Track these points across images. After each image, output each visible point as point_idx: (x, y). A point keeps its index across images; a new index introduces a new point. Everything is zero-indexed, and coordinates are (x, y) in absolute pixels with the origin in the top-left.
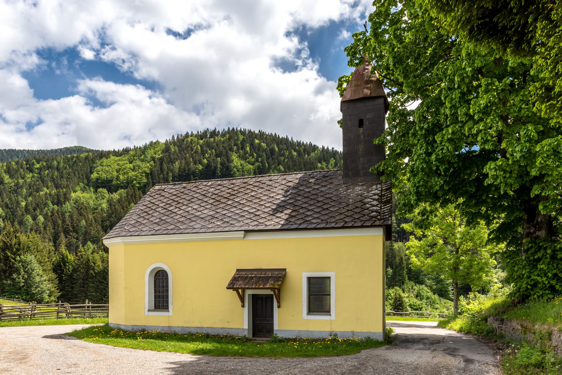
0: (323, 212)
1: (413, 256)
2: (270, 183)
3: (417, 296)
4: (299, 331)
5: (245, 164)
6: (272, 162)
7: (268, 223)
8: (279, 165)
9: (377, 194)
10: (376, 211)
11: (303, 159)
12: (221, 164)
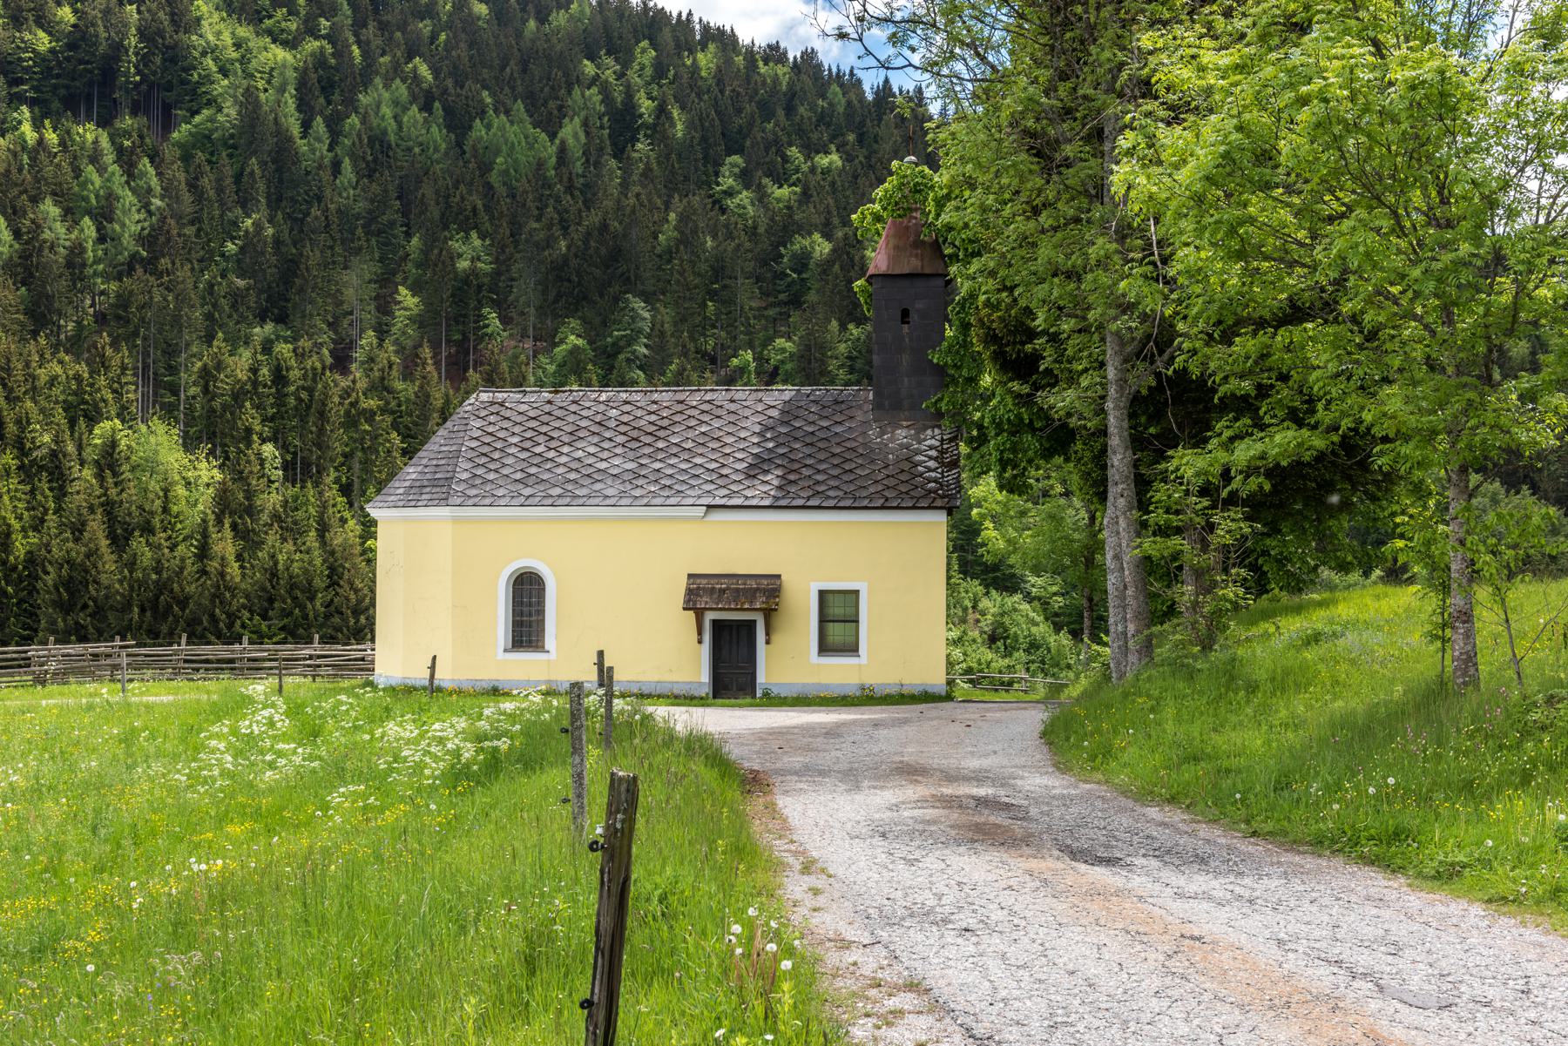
0: (846, 478)
1: (988, 524)
2: (733, 407)
3: (992, 639)
4: (804, 685)
5: (255, 43)
6: (379, 41)
7: (749, 493)
8: (410, 59)
9: (935, 448)
10: (935, 481)
11: (519, 34)
12: (142, 33)
